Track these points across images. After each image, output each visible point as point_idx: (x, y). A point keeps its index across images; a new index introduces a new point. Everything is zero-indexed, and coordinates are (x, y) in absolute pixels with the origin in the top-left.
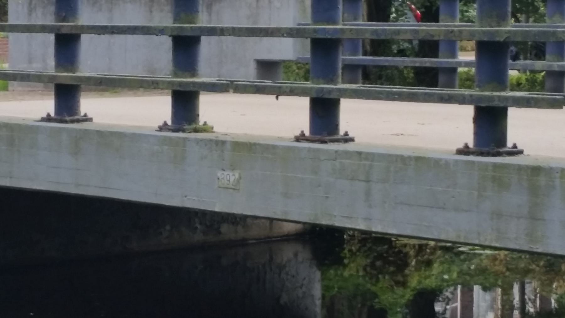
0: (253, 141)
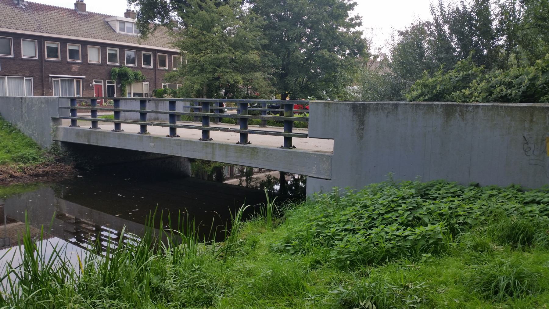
0: (268, 148)
